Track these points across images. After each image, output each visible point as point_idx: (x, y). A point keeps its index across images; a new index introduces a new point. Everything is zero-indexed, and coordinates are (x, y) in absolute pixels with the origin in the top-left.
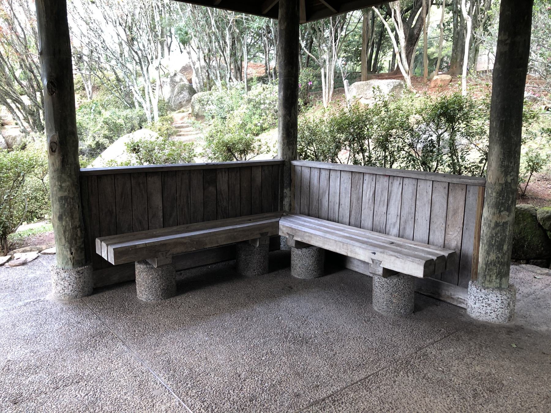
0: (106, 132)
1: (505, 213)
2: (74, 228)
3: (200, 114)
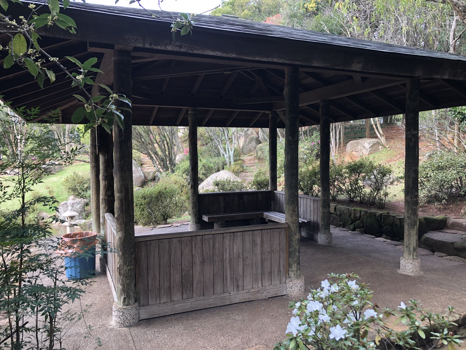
0: (204, 172)
1: (325, 209)
2: (196, 212)
3: (261, 157)
